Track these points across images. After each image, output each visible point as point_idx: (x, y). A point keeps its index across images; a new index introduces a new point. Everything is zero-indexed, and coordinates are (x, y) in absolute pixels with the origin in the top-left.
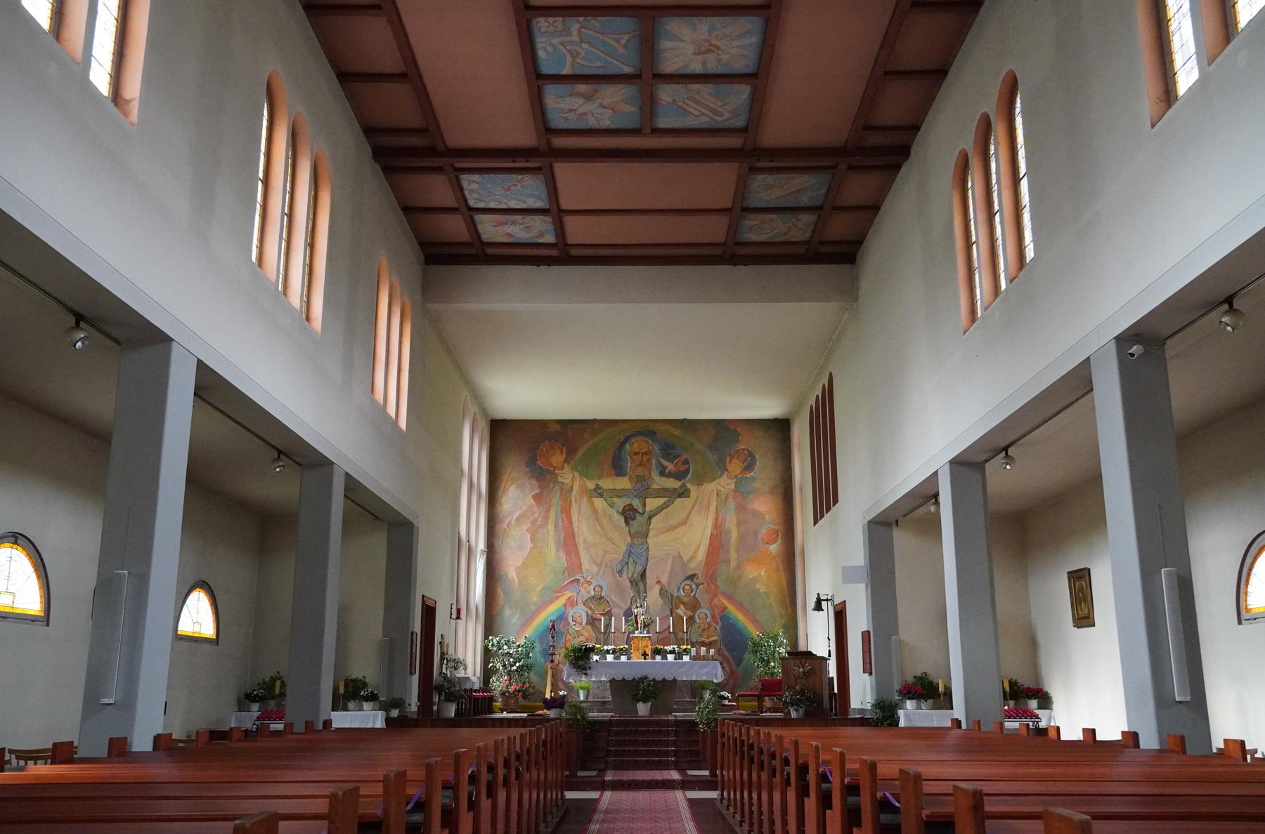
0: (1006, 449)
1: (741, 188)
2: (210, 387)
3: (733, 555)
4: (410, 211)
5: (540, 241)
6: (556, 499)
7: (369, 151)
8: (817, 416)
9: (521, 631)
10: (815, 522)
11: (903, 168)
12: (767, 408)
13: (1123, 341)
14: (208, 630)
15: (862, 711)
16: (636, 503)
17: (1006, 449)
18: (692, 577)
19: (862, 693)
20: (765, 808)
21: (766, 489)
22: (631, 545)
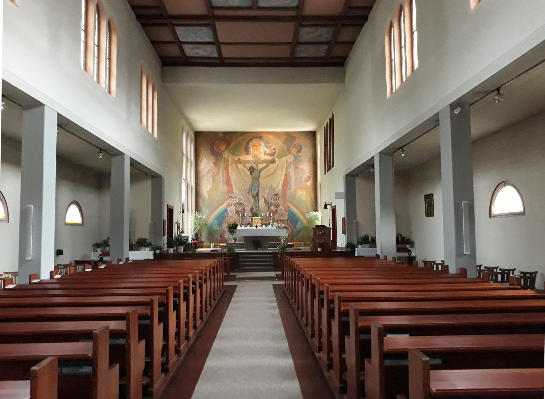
0: (402, 148)
1: (296, 34)
2: (64, 124)
3: (293, 187)
4: (155, 43)
5: (211, 56)
6: (222, 165)
7: (134, 16)
8: (330, 127)
9: (210, 216)
10: (325, 173)
11: (365, 25)
12: (309, 127)
13: (453, 106)
14: (79, 220)
15: (341, 248)
16: (255, 166)
17: (402, 148)
18: (277, 195)
19: (342, 241)
20: (300, 294)
21: (306, 159)
22: (252, 183)
